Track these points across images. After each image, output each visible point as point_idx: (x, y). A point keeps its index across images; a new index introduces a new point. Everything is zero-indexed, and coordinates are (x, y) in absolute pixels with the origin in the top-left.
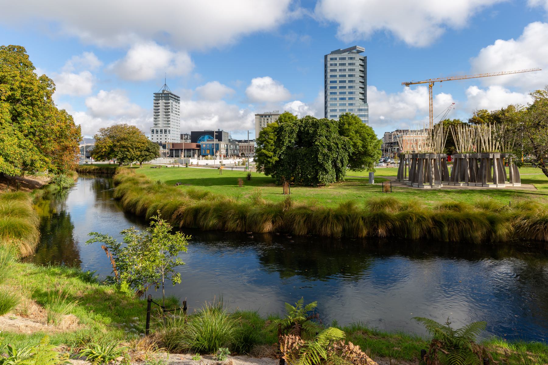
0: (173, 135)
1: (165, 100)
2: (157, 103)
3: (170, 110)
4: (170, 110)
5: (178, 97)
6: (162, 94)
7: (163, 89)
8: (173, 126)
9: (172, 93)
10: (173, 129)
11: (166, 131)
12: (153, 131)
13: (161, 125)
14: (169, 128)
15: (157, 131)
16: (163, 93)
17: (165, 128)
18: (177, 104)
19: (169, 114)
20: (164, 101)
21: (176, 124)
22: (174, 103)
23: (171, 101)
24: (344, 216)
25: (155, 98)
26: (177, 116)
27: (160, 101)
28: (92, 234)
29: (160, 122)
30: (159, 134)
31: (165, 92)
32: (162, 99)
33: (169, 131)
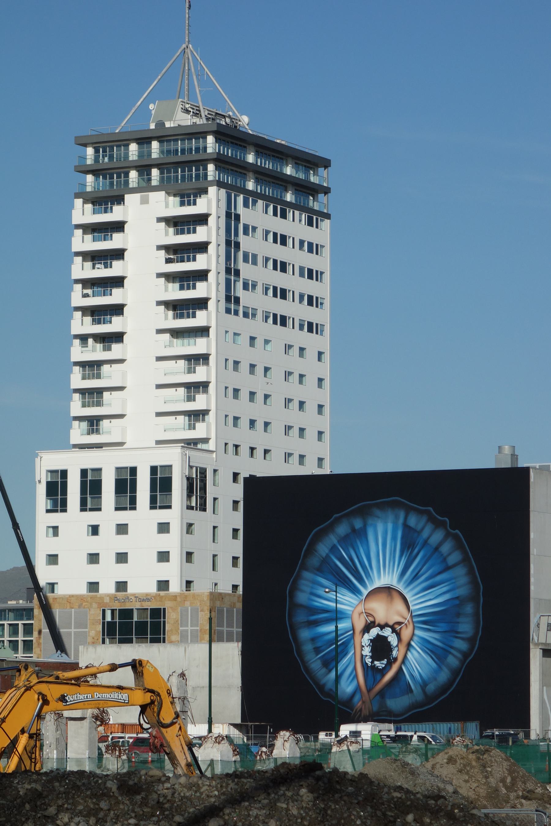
18: (295, 226)
21: (279, 389)
30: (108, 515)
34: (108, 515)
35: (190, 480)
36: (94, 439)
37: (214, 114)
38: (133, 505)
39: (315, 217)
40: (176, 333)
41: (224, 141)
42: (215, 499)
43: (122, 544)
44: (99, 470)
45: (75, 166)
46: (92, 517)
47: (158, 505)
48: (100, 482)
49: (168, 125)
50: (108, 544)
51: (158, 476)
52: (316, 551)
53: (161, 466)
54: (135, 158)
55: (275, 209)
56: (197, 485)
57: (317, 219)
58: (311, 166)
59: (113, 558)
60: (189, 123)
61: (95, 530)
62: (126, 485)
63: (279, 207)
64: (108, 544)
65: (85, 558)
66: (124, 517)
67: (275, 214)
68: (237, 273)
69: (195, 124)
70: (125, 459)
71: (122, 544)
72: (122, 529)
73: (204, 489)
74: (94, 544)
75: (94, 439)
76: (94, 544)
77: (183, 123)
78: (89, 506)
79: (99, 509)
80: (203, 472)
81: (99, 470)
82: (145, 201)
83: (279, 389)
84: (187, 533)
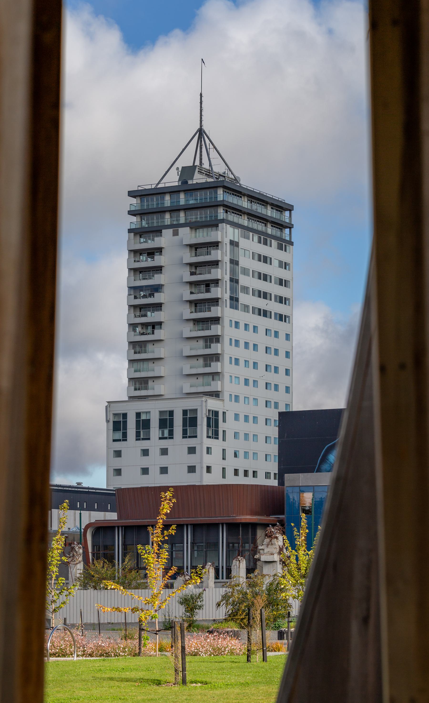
0: (241, 445)
1: (195, 226)
2: (151, 253)
3: (222, 292)
4: (222, 292)
5: (281, 207)
6: (173, 191)
7: (187, 160)
8: (241, 390)
9: (247, 182)
10: (241, 408)
11: (190, 420)
12: (119, 425)
13: (171, 391)
14: (213, 404)
15: (143, 425)
16: (185, 187)
17: (190, 404)
18: (271, 250)
19: (215, 311)
20: (187, 235)
21: (262, 358)
22: (250, 245)
23: (227, 234)
24: (90, 508)
25: (134, 221)
26: (273, 324)
27: (166, 239)
28: (218, 605)
29: (160, 369)
30: (155, 443)
31: (198, 179)
32: (175, 227)
33: (213, 420)
34: (155, 443)
35: (208, 419)
36: (143, 393)
37: (218, 175)
38: (171, 435)
39: (284, 244)
40: (196, 321)
41: (228, 193)
42: (224, 431)
43: (164, 461)
44: (196, 410)
45: (128, 211)
46: (145, 444)
47: (188, 435)
48: (149, 420)
49: (190, 182)
50: (155, 461)
51: (188, 416)
52: (328, 460)
53: (190, 410)
54: (169, 205)
55: (260, 239)
56: (212, 423)
57: (285, 246)
58: (264, 204)
59: (158, 470)
60: (204, 181)
61: (145, 452)
62: (166, 422)
63: (262, 237)
64: (155, 461)
65: (139, 471)
66: (165, 444)
67: (260, 242)
68: (237, 281)
69: (207, 183)
70: (166, 406)
71: (164, 461)
72: (164, 452)
73: (217, 426)
74: (145, 462)
75: (143, 393)
76: (145, 462)
77: (199, 181)
78: (142, 437)
79: (149, 439)
80: (216, 413)
81: (196, 410)
82: (176, 234)
83: (262, 358)
84: (207, 454)
